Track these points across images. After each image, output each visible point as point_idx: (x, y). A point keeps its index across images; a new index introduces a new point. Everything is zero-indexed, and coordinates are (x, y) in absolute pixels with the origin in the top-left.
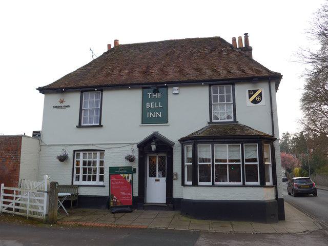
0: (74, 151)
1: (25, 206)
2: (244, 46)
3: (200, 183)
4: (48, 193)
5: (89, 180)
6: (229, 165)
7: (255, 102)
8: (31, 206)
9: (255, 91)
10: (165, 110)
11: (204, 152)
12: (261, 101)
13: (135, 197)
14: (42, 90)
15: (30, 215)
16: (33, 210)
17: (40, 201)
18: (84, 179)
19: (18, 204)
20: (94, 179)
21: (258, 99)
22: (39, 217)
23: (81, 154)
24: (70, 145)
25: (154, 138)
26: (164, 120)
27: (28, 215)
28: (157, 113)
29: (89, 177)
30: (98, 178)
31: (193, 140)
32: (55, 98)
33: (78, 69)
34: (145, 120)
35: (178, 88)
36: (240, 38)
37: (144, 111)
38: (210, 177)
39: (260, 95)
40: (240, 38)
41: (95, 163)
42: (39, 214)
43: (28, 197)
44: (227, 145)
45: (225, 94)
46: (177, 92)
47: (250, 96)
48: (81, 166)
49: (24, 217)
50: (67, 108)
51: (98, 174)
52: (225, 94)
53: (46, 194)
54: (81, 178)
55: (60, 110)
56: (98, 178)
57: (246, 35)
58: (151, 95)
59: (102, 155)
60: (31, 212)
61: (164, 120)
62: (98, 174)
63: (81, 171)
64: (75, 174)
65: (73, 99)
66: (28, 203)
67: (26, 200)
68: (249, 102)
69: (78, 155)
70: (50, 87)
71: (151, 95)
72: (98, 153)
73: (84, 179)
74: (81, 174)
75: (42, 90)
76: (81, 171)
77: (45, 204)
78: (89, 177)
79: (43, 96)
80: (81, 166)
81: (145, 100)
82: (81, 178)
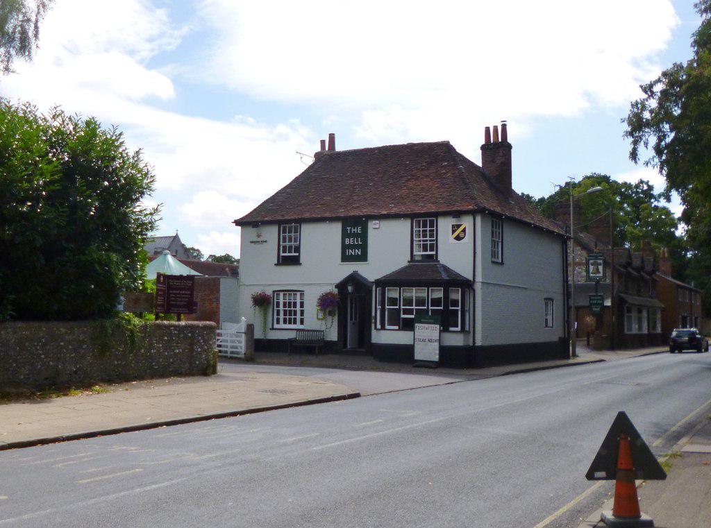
0: (274, 291)
1: (227, 347)
2: (500, 140)
3: (387, 327)
4: (245, 333)
5: (290, 323)
6: (416, 309)
7: (458, 238)
8: (232, 347)
9: (459, 226)
10: (364, 247)
11: (393, 293)
12: (463, 238)
13: (607, 474)
14: (237, 223)
15: (231, 355)
16: (232, 344)
17: (240, 342)
18: (285, 322)
19: (219, 346)
20: (295, 323)
21: (462, 235)
22: (239, 356)
23: (282, 294)
24: (270, 285)
25: (354, 279)
26: (363, 258)
27: (229, 355)
28: (350, 251)
29: (290, 319)
30: (298, 321)
31: (383, 283)
32: (252, 232)
33: (277, 193)
34: (345, 258)
35: (377, 222)
36: (496, 128)
37: (344, 247)
38: (347, 310)
39: (464, 230)
40: (496, 128)
41: (295, 304)
42: (238, 353)
43: (229, 338)
44: (414, 288)
45: (428, 229)
46: (377, 226)
47: (453, 232)
48: (281, 308)
49: (226, 357)
50: (264, 243)
51: (298, 317)
52: (428, 229)
53: (243, 335)
54: (281, 321)
55: (258, 246)
56: (298, 321)
57: (504, 127)
58: (351, 230)
59: (302, 295)
60: (232, 353)
61: (363, 258)
62: (298, 317)
63: (282, 313)
64: (275, 317)
65: (271, 233)
66: (229, 344)
67: (227, 341)
68: (451, 238)
69: (278, 295)
70: (249, 220)
71: (351, 230)
72: (298, 294)
73: (285, 322)
74: (282, 317)
75: (237, 223)
76: (282, 313)
77: (243, 345)
78: (290, 319)
79: (239, 228)
80: (281, 308)
81: (345, 235)
82: (281, 321)
